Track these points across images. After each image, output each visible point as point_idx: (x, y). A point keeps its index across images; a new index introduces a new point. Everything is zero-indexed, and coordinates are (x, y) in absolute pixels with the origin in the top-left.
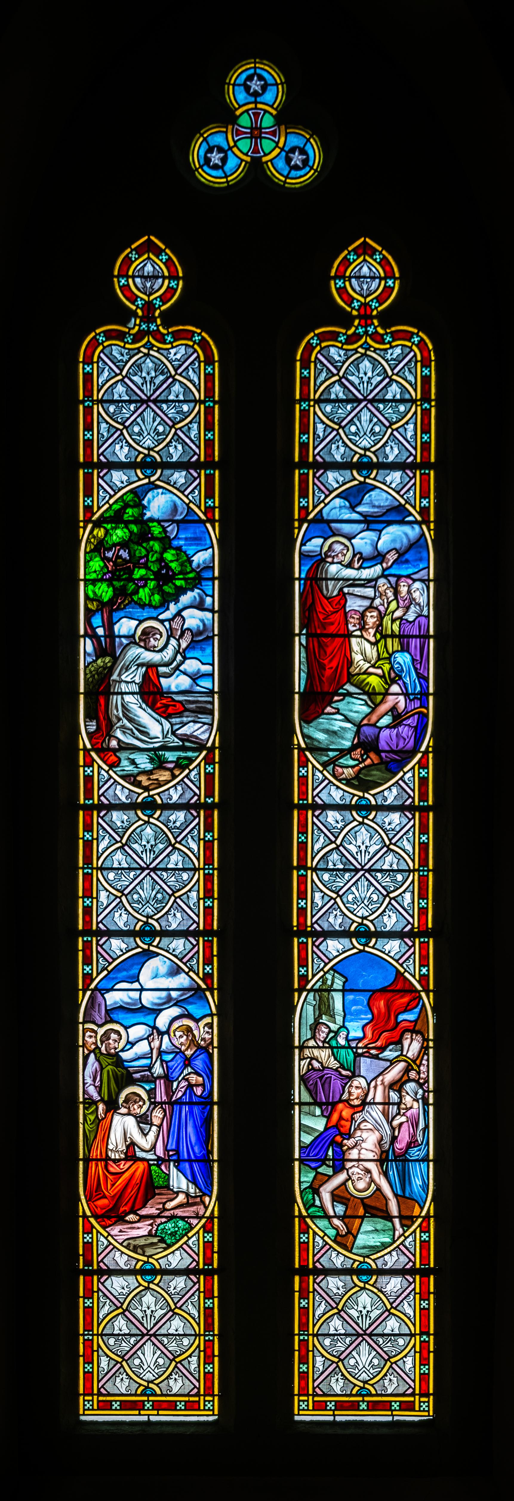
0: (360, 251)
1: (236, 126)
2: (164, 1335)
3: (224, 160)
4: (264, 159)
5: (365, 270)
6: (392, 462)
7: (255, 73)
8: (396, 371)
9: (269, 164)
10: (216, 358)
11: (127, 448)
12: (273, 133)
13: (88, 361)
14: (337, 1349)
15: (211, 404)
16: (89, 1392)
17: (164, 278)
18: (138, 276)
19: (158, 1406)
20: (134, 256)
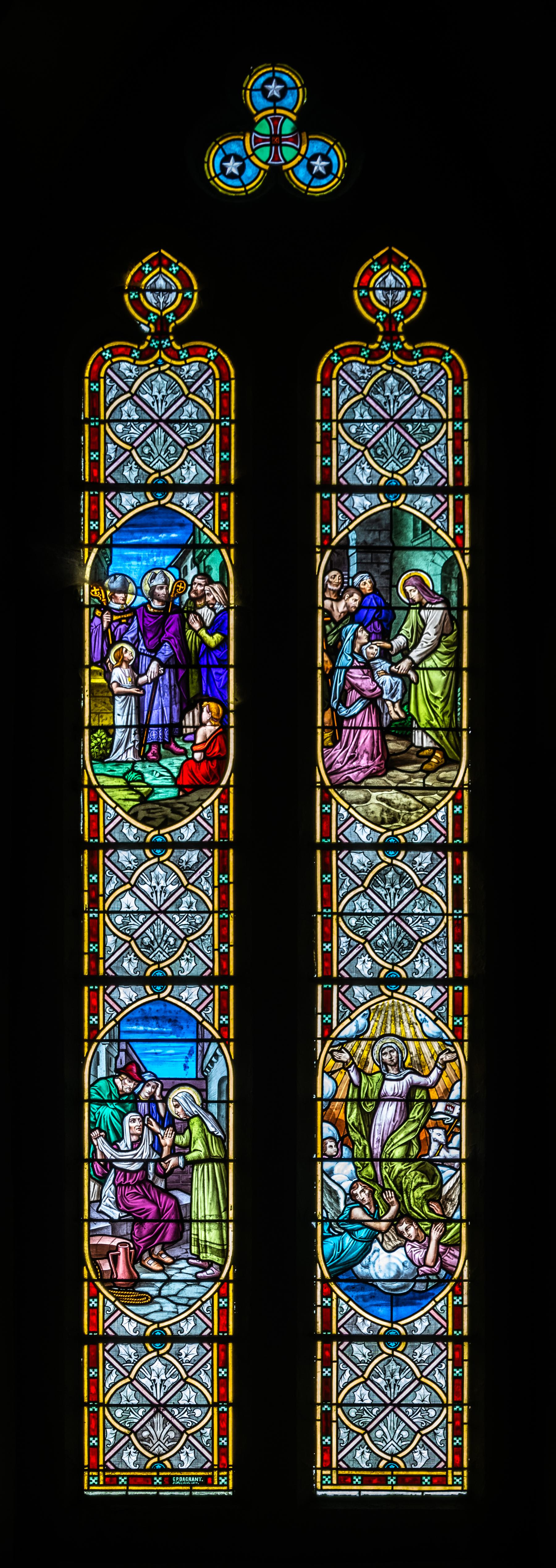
0: (155, 263)
1: (254, 134)
2: (174, 1406)
3: (242, 169)
4: (285, 167)
5: (161, 283)
6: (421, 486)
7: (274, 77)
8: (192, 390)
9: (290, 171)
10: (232, 376)
11: (369, 471)
12: (294, 140)
13: (94, 378)
14: (363, 1420)
15: (228, 424)
16: (94, 1467)
17: (406, 289)
18: (380, 289)
19: (401, 1481)
20: (147, 269)
